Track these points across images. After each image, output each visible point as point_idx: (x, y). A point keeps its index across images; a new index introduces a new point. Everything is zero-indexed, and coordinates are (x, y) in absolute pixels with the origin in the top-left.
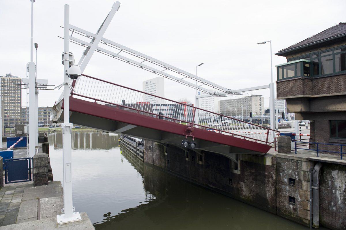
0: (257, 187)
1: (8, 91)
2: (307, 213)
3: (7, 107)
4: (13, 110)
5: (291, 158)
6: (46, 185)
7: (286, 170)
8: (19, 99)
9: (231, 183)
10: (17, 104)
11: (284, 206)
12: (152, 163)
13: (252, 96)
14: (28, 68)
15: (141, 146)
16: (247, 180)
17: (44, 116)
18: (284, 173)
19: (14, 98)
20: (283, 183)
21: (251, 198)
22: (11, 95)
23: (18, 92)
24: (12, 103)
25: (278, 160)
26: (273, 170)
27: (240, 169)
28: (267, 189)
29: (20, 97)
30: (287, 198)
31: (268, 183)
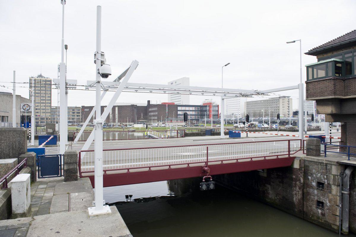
1: (39, 92)
2: (336, 219)
3: (38, 107)
4: (43, 109)
5: (320, 161)
7: (314, 173)
10: (48, 104)
13: (280, 98)
14: (59, 68)
17: (73, 116)
18: (313, 176)
20: (311, 186)
24: (43, 103)
25: (307, 163)
27: (266, 172)
30: (315, 203)
31: (295, 187)
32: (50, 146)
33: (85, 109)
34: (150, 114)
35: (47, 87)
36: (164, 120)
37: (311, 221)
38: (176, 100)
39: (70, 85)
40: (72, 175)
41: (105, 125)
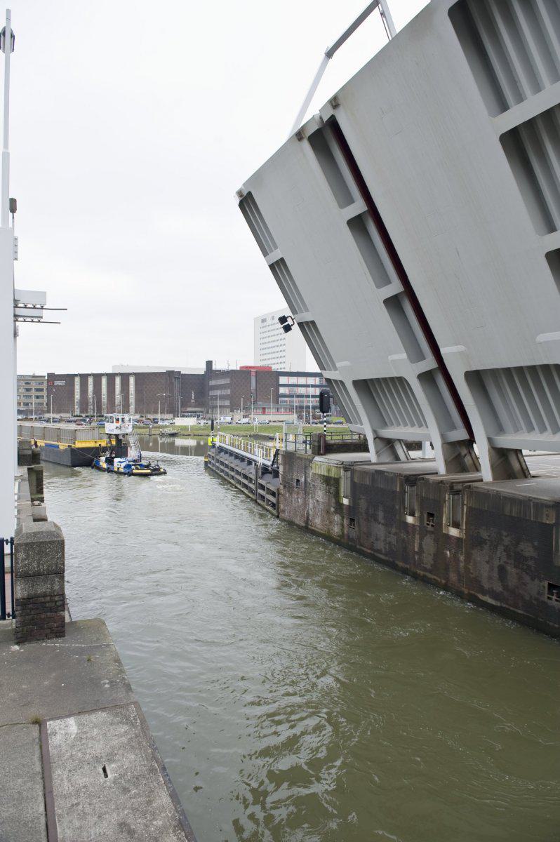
15: (269, 477)
34: (211, 393)
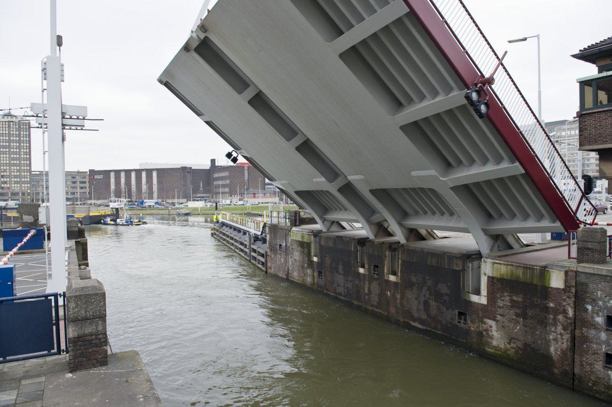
0: (526, 332)
1: (7, 144)
3: (6, 172)
4: (16, 177)
6: (101, 365)
7: (600, 299)
8: (27, 158)
9: (462, 321)
10: (24, 166)
11: (592, 372)
12: (285, 277)
14: (44, 70)
15: (259, 243)
16: (501, 315)
17: (73, 187)
18: (597, 304)
19: (18, 156)
20: (594, 325)
21: (511, 352)
22: (12, 150)
23: (25, 145)
24: (15, 165)
25: (582, 279)
26: (569, 298)
27: (486, 294)
28: (551, 337)
29: (28, 153)
30: (602, 358)
31: (555, 325)
32: (29, 253)
33: (95, 175)
34: (215, 183)
35: (22, 136)
36: (242, 194)
37: (592, 394)
38: (528, 120)
39: (71, 118)
40: (90, 350)
41: (134, 205)
